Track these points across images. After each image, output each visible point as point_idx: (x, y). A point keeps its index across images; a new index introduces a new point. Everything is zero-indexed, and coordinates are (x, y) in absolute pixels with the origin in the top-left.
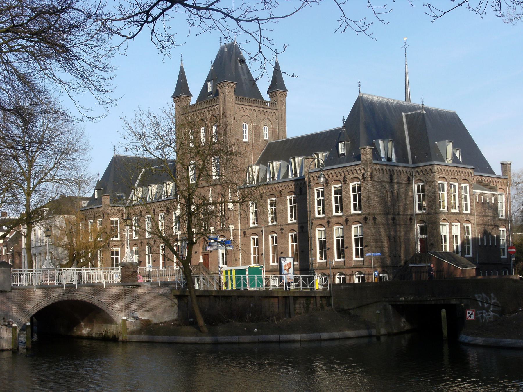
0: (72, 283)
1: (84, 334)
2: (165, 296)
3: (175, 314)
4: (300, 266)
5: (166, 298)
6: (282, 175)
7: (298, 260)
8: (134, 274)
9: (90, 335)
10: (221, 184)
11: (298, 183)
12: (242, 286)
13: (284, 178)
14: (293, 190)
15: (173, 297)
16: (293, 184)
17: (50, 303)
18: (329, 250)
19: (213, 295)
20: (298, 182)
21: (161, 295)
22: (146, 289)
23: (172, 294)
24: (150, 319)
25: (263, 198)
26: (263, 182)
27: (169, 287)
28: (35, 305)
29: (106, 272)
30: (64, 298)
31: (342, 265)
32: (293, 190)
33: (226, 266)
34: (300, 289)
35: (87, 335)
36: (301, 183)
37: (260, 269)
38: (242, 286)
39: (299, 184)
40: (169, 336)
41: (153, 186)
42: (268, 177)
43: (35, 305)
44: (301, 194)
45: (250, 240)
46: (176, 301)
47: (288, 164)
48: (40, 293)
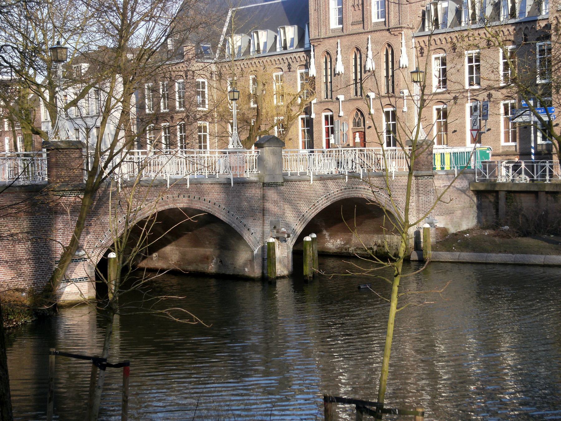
0: (353, 172)
1: (330, 249)
2: (463, 191)
3: (474, 218)
4: (520, 149)
5: (463, 195)
6: (268, 48)
7: (518, 140)
8: (429, 157)
9: (344, 251)
10: (388, 30)
11: (520, 29)
12: (548, 178)
13: (453, 25)
14: (512, 38)
15: (471, 193)
16: (511, 29)
17: (329, 204)
18: (489, 132)
19: (547, 190)
20: (521, 26)
21: (458, 189)
22: (441, 182)
23: (472, 189)
24: (447, 227)
25: (456, 51)
26: (456, 26)
27: (466, 178)
28: (312, 207)
29: (293, 155)
30: (346, 195)
31: (512, 151)
32: (512, 38)
33: (445, 146)
34: (546, 180)
35: (336, 251)
36: (527, 28)
37: (488, 152)
38: (548, 178)
39: (523, 29)
40: (512, 253)
41: (260, 32)
42: (252, 49)
43: (312, 207)
44: (290, 71)
45: (432, 111)
46: (475, 199)
47: (276, 34)
48: (318, 186)
